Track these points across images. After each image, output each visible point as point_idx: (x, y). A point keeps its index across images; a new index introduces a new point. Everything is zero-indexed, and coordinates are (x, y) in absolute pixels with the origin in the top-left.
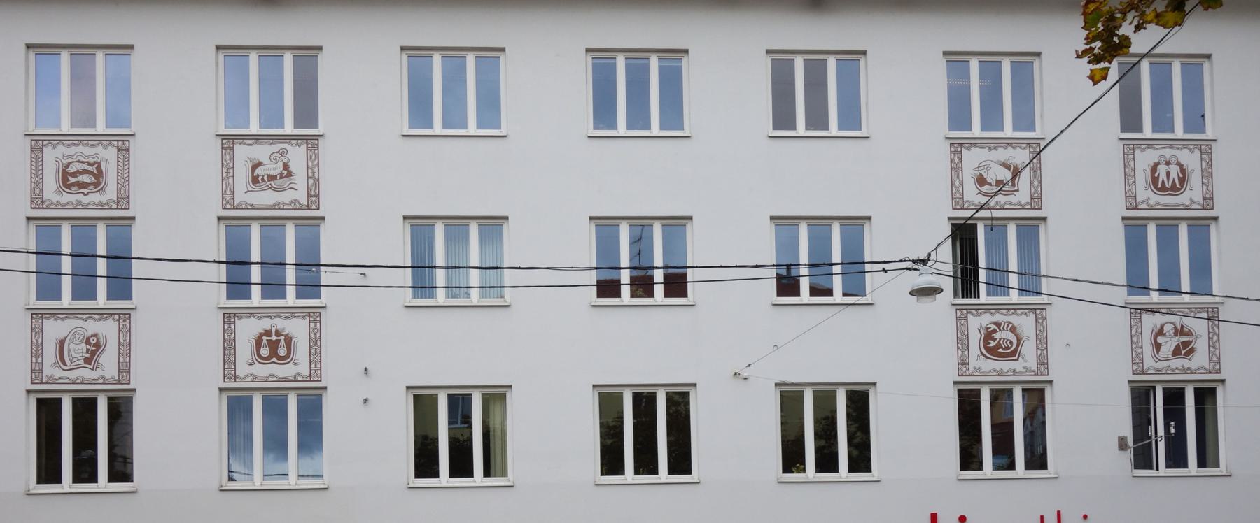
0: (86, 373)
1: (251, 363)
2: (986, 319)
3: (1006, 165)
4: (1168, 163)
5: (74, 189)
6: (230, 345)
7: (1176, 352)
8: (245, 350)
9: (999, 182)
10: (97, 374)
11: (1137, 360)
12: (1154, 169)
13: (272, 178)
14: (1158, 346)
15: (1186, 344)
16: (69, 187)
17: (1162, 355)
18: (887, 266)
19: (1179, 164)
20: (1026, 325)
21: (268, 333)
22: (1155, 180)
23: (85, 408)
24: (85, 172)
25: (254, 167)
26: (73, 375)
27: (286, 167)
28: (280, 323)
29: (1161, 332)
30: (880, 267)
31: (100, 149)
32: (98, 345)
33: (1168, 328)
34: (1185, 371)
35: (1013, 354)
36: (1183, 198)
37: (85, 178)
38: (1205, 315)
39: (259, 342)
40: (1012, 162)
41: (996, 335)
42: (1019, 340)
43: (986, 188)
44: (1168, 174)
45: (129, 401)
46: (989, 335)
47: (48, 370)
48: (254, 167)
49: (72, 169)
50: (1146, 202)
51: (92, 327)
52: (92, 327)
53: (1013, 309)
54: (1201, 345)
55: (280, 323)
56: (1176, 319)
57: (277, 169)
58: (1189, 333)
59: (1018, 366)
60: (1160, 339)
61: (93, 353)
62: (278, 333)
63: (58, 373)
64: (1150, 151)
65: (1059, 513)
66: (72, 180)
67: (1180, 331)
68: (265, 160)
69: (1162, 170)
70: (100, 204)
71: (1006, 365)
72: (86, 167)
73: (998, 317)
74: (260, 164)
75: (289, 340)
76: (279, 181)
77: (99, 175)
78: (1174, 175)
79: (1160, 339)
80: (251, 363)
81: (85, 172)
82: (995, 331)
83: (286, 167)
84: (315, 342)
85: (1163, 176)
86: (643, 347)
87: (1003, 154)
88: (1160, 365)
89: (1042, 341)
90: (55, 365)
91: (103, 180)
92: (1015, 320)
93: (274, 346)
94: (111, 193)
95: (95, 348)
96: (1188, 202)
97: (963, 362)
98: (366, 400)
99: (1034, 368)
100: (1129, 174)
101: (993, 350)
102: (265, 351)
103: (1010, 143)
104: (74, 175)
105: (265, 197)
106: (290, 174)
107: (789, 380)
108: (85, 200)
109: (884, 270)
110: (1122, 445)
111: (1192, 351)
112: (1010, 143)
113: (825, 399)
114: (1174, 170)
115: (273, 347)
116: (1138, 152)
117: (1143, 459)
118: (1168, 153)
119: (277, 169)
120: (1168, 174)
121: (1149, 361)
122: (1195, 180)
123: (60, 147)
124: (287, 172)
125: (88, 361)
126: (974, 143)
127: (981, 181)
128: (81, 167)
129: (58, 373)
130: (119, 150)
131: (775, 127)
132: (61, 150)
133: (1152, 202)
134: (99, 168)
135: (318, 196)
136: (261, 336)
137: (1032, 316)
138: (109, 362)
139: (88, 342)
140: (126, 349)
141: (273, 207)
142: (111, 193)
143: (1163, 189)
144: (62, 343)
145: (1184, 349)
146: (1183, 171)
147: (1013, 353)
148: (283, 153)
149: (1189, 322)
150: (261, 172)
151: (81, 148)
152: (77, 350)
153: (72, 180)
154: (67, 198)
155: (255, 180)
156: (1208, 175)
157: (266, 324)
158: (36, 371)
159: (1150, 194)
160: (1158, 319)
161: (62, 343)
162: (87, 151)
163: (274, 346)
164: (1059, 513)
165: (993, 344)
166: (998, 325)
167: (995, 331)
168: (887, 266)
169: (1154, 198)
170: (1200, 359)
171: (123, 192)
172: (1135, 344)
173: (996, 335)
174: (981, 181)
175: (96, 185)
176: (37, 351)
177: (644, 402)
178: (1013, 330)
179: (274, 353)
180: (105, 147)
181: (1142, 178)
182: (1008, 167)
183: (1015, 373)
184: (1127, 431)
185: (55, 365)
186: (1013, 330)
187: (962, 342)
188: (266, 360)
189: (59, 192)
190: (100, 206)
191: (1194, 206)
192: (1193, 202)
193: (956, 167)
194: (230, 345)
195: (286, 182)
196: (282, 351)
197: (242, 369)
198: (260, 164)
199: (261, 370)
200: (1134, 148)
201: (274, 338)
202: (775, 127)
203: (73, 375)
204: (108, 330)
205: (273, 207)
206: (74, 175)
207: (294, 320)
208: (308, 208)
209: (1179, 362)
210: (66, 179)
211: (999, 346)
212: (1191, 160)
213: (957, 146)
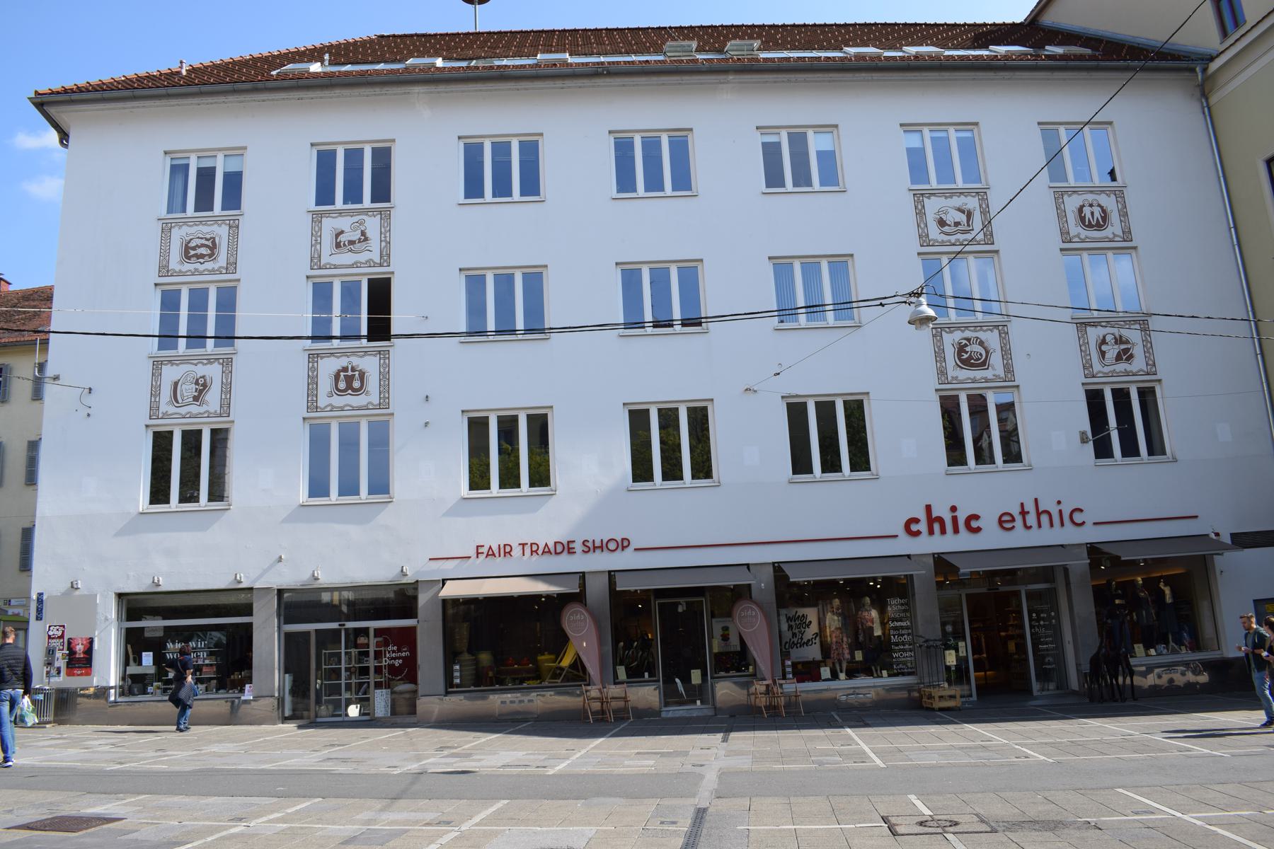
0: (194, 409)
1: (330, 395)
2: (958, 336)
3: (960, 210)
4: (1091, 205)
5: (193, 260)
6: (313, 381)
7: (1118, 358)
8: (325, 384)
9: (957, 224)
10: (202, 409)
11: (1087, 366)
12: (1081, 210)
13: (352, 243)
14: (1103, 354)
15: (1126, 351)
16: (189, 258)
17: (1107, 361)
18: (884, 302)
19: (1099, 205)
20: (992, 339)
21: (345, 369)
22: (1082, 219)
23: (191, 440)
24: (203, 245)
25: (337, 235)
26: (183, 411)
27: (363, 233)
28: (355, 361)
29: (1104, 342)
30: (878, 302)
31: (215, 228)
32: (205, 385)
33: (1108, 338)
34: (1127, 373)
35: (984, 364)
36: (1108, 232)
37: (203, 251)
38: (1137, 326)
39: (337, 377)
40: (966, 208)
41: (968, 349)
42: (987, 352)
43: (946, 229)
44: (1092, 214)
45: (227, 431)
46: (961, 349)
47: (164, 408)
48: (337, 235)
49: (192, 244)
50: (1078, 235)
51: (201, 370)
52: (201, 370)
53: (979, 327)
54: (1138, 351)
55: (355, 361)
56: (1115, 331)
57: (356, 236)
58: (1127, 342)
59: (988, 374)
60: (1104, 348)
61: (201, 392)
62: (353, 370)
63: (171, 410)
64: (1075, 196)
65: (1036, 500)
66: (192, 252)
67: (1119, 340)
68: (347, 229)
69: (1087, 211)
70: (213, 270)
71: (978, 374)
72: (204, 242)
73: (968, 334)
74: (342, 232)
75: (362, 375)
76: (358, 245)
77: (213, 247)
78: (1097, 215)
79: (1104, 348)
80: (330, 395)
81: (203, 245)
82: (966, 345)
83: (363, 233)
84: (385, 377)
85: (1088, 216)
86: (667, 371)
87: (958, 201)
88: (1106, 369)
89: (1006, 352)
90: (170, 403)
91: (216, 251)
92: (982, 335)
93: (349, 380)
94: (222, 260)
95: (202, 386)
96: (1111, 236)
97: (942, 372)
98: (427, 424)
99: (1002, 375)
100: (1062, 215)
101: (966, 362)
102: (342, 385)
103: (962, 193)
104: (194, 248)
105: (346, 258)
106: (366, 239)
107: (794, 392)
108: (201, 267)
109: (881, 305)
110: (1084, 440)
111: (1131, 356)
112: (962, 193)
113: (669, 418)
114: (1097, 211)
115: (349, 381)
116: (1065, 197)
117: (1103, 450)
118: (1090, 197)
119: (356, 236)
120: (1092, 214)
121: (1097, 367)
122: (1114, 217)
123: (184, 227)
124: (364, 238)
125: (196, 399)
126: (932, 194)
127: (942, 223)
128: (200, 242)
129: (171, 410)
130: (230, 227)
131: (768, 186)
132: (185, 229)
133: (1082, 237)
134: (214, 242)
135: (389, 256)
136: (339, 371)
137: (996, 332)
138: (213, 398)
139: (197, 383)
140: (227, 388)
141: (351, 266)
142: (222, 260)
143: (1090, 226)
144: (176, 384)
145: (1125, 356)
146: (1104, 211)
147: (984, 364)
148: (361, 223)
149: (1126, 333)
150: (342, 238)
151: (201, 227)
152: (188, 390)
153: (192, 252)
154: (188, 267)
155: (338, 245)
156: (1124, 214)
157: (344, 362)
158: (154, 411)
159: (1080, 230)
160: (1100, 331)
161: (176, 384)
162: (205, 229)
163: (349, 380)
164: (1036, 500)
165: (965, 356)
166: (969, 340)
167: (966, 345)
168: (884, 302)
169: (1084, 233)
170: (1138, 363)
171: (232, 260)
172: (1084, 352)
173: (968, 349)
174: (942, 223)
175: (212, 254)
176: (155, 392)
177: (826, 409)
178: (981, 343)
179: (349, 386)
180: (220, 225)
181: (1072, 218)
182: (963, 212)
183: (987, 381)
184: (1087, 427)
185: (170, 403)
186: (981, 343)
187: (939, 355)
188: (340, 392)
189: (182, 263)
190: (212, 272)
191: (931, 824)
192: (1115, 235)
193: (920, 213)
194: (313, 381)
195: (363, 245)
196: (356, 384)
197: (323, 401)
198: (342, 232)
199: (338, 401)
200: (1062, 194)
201: (350, 373)
202: (768, 186)
203: (183, 411)
204: (214, 372)
205: (351, 266)
206: (194, 248)
207: (367, 358)
208: (381, 265)
209: (1121, 367)
210: (188, 252)
211: (970, 358)
212: (1109, 203)
213: (919, 197)
